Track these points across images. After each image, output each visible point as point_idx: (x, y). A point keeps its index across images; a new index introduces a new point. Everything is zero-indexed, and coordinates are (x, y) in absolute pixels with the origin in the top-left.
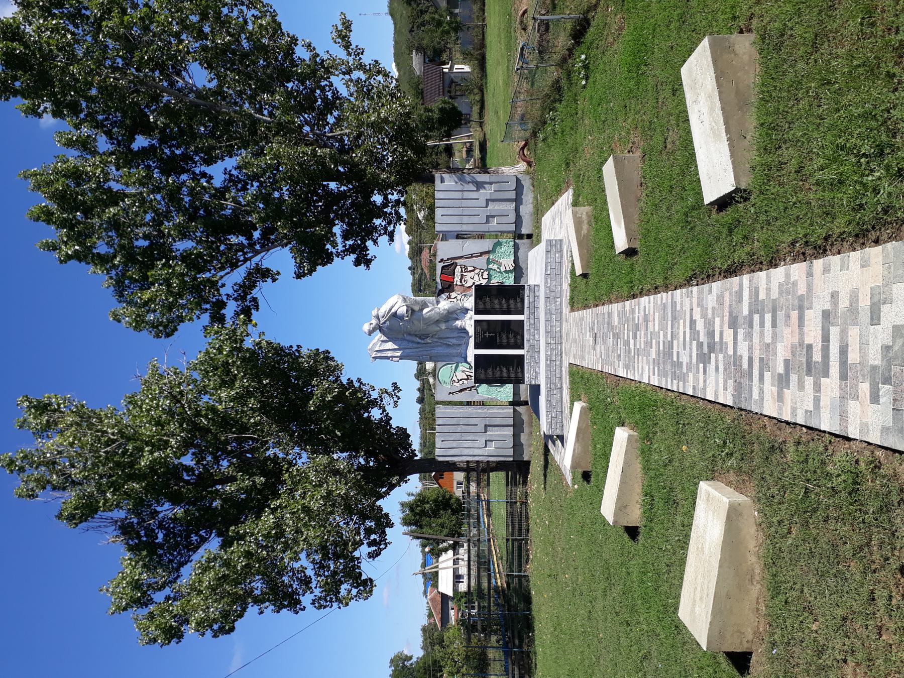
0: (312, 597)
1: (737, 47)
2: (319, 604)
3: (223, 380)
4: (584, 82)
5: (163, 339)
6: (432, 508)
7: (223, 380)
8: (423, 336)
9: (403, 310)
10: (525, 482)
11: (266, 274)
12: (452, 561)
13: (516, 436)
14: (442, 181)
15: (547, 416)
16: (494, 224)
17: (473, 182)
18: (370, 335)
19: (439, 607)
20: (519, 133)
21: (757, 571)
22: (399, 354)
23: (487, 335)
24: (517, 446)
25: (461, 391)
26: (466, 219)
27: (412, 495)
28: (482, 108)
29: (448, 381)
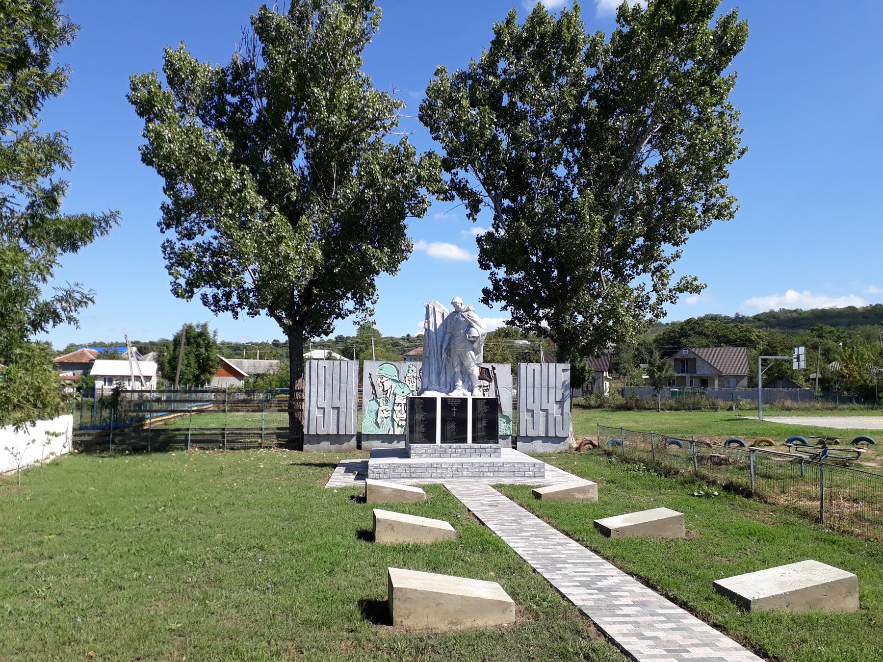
0: (174, 240)
1: (850, 598)
2: (167, 247)
3: (387, 167)
4: (696, 494)
5: (417, 112)
6: (201, 354)
7: (387, 167)
8: (448, 351)
9: (475, 333)
10: (281, 446)
11: (474, 207)
12: (138, 374)
13: (538, 438)
14: (564, 370)
15: (386, 465)
16: (525, 417)
17: (563, 399)
18: (452, 303)
19: (75, 361)
20: (606, 441)
21: (459, 628)
22: (432, 328)
23: (454, 409)
24: (318, 438)
25: (372, 385)
26: (530, 391)
27: (215, 335)
28: (584, 407)
29: (382, 373)
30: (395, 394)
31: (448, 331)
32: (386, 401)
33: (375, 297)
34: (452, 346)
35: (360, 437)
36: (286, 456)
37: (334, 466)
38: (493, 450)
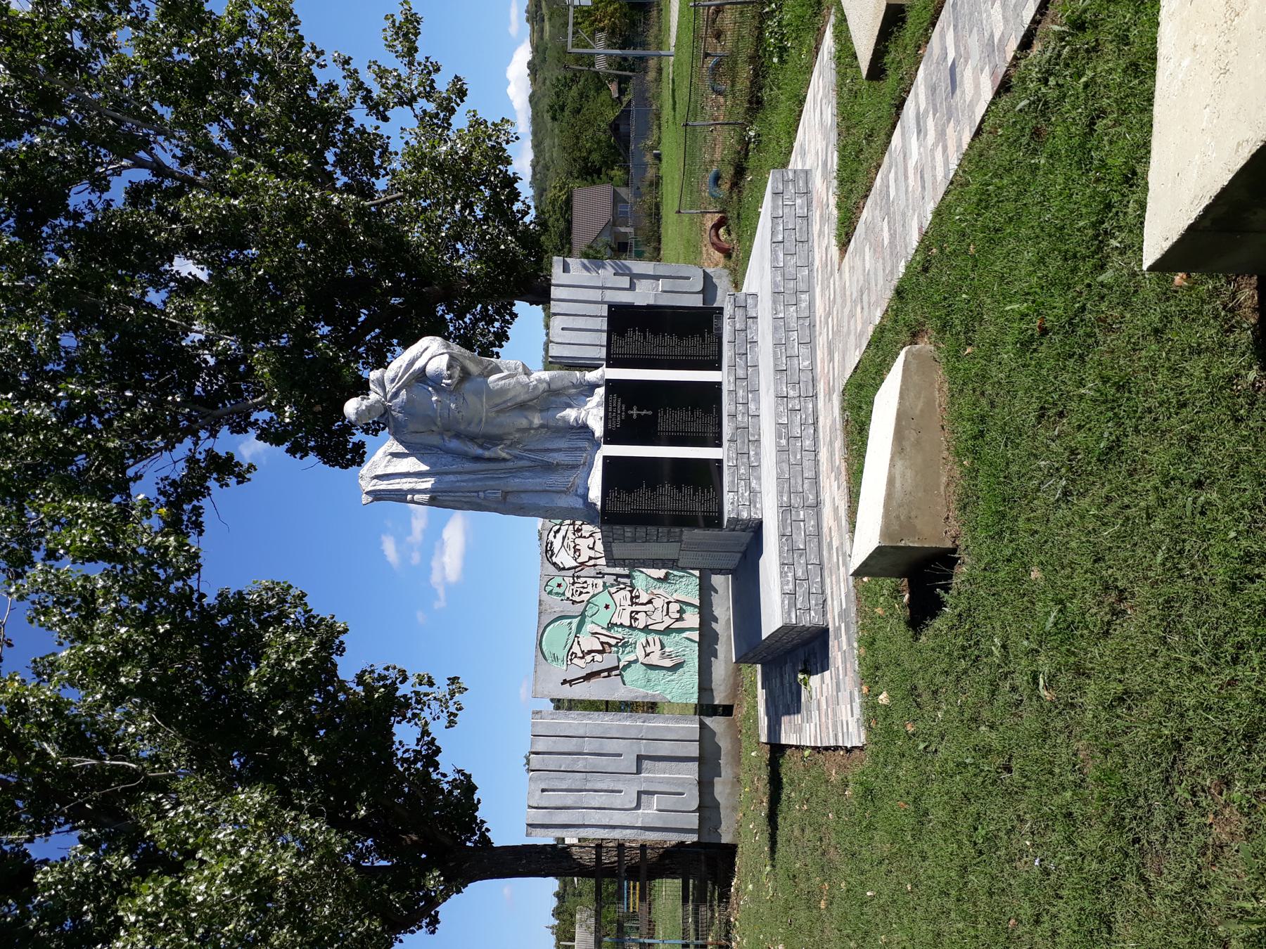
8: (491, 440)
10: (725, 897)
11: (225, 467)
13: (705, 785)
14: (566, 269)
15: (783, 575)
22: (428, 484)
23: (634, 412)
24: (708, 808)
25: (588, 677)
29: (562, 654)
30: (611, 626)
31: (435, 440)
32: (625, 645)
33: (392, 674)
34: (473, 429)
35: (706, 708)
36: (751, 884)
37: (777, 750)
38: (739, 312)
